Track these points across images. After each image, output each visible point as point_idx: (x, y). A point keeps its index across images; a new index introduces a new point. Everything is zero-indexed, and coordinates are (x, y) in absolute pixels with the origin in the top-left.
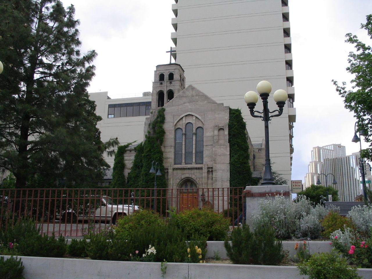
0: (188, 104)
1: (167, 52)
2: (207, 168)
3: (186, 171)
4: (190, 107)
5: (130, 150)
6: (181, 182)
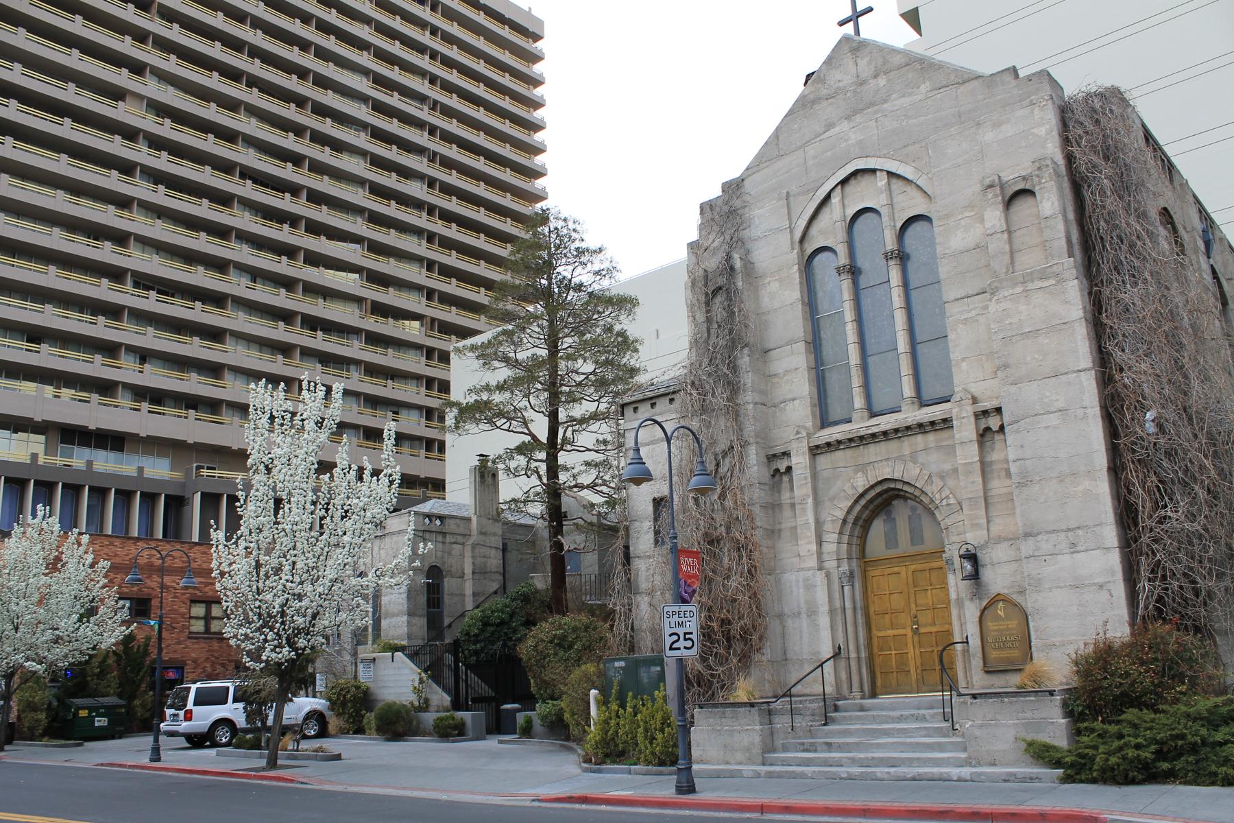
0: (844, 126)
1: (870, 10)
2: (972, 419)
3: (873, 452)
4: (854, 137)
5: (651, 398)
6: (858, 508)
